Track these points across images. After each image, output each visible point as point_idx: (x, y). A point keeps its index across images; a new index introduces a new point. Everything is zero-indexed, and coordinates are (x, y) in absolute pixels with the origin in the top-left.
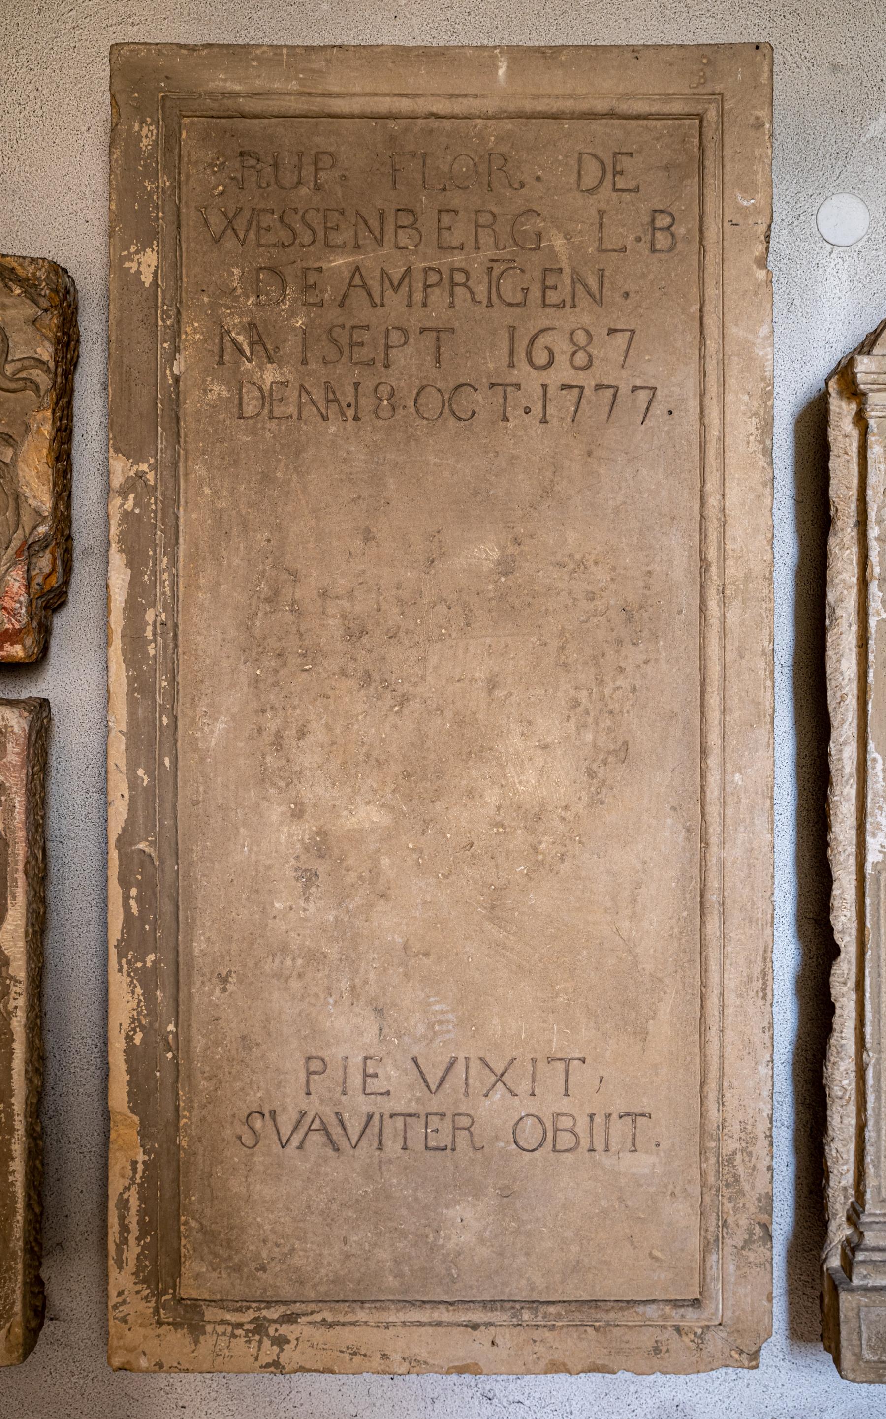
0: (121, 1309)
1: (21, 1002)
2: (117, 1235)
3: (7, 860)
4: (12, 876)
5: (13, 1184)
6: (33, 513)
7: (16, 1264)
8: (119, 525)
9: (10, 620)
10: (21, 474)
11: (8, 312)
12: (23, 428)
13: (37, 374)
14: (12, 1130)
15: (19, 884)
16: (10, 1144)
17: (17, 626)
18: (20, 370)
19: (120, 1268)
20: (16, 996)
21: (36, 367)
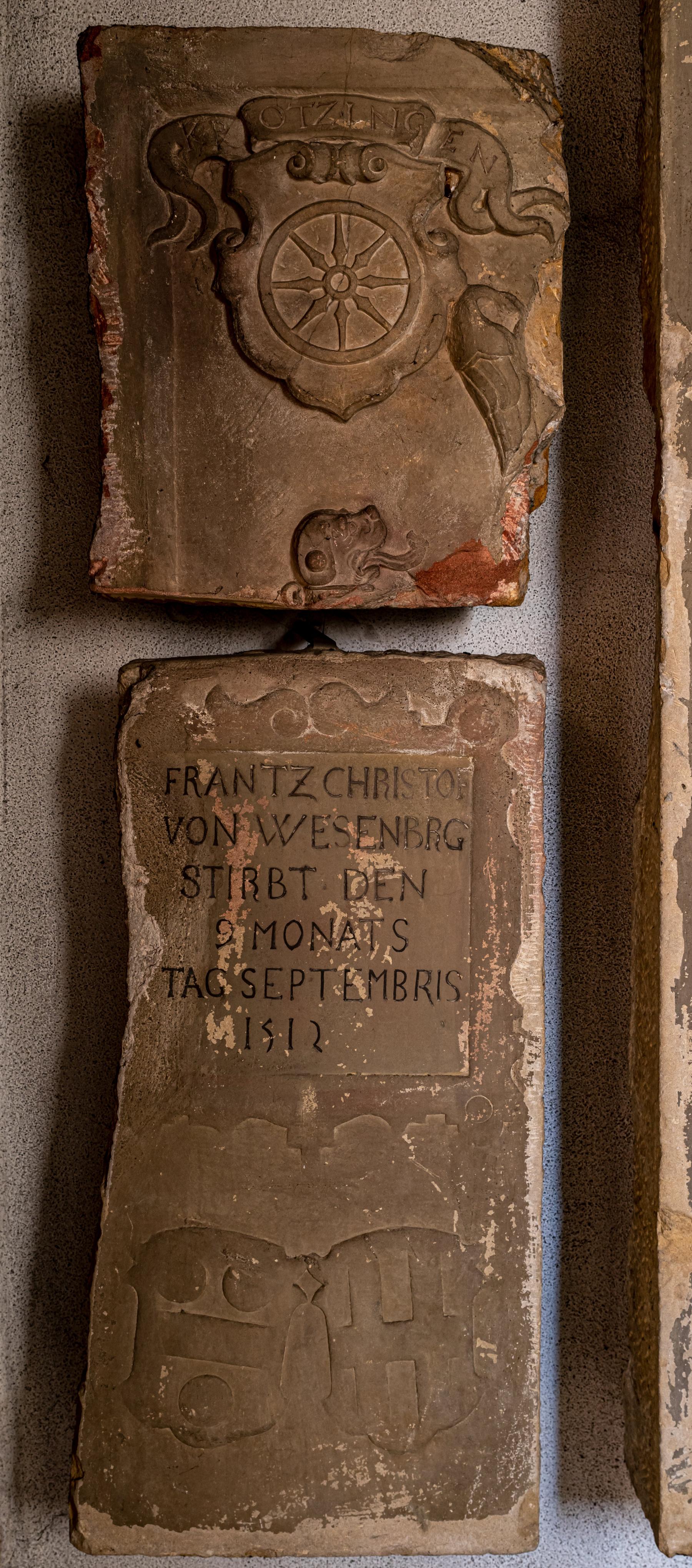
0: (678, 1474)
1: (537, 1066)
2: (673, 1376)
3: (520, 875)
4: (526, 897)
5: (526, 1311)
6: (548, 402)
7: (531, 1417)
8: (679, 420)
9: (508, 549)
10: (527, 347)
11: (507, 125)
12: (531, 285)
13: (547, 210)
14: (525, 1239)
15: (536, 907)
16: (524, 1256)
17: (516, 558)
18: (528, 206)
19: (677, 1419)
20: (531, 1059)
21: (545, 201)
